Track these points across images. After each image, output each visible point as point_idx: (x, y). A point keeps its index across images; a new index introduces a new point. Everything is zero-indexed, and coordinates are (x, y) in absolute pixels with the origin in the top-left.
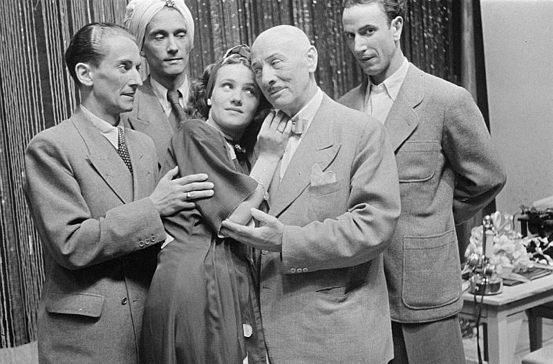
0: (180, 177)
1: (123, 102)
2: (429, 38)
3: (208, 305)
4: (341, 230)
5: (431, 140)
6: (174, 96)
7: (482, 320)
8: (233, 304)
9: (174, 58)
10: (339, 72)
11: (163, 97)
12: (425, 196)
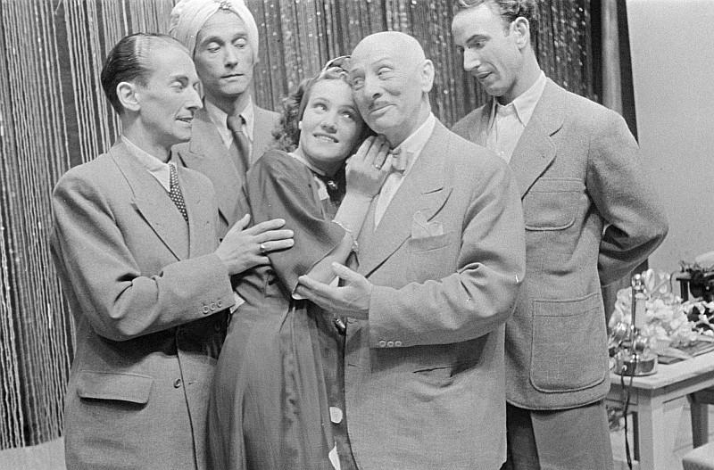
0: (254, 225)
1: (179, 129)
2: (561, 47)
3: (284, 385)
4: (444, 294)
5: (571, 178)
6: (236, 123)
7: (631, 408)
8: (316, 382)
9: (233, 73)
10: (446, 92)
11: (221, 124)
12: (562, 248)
